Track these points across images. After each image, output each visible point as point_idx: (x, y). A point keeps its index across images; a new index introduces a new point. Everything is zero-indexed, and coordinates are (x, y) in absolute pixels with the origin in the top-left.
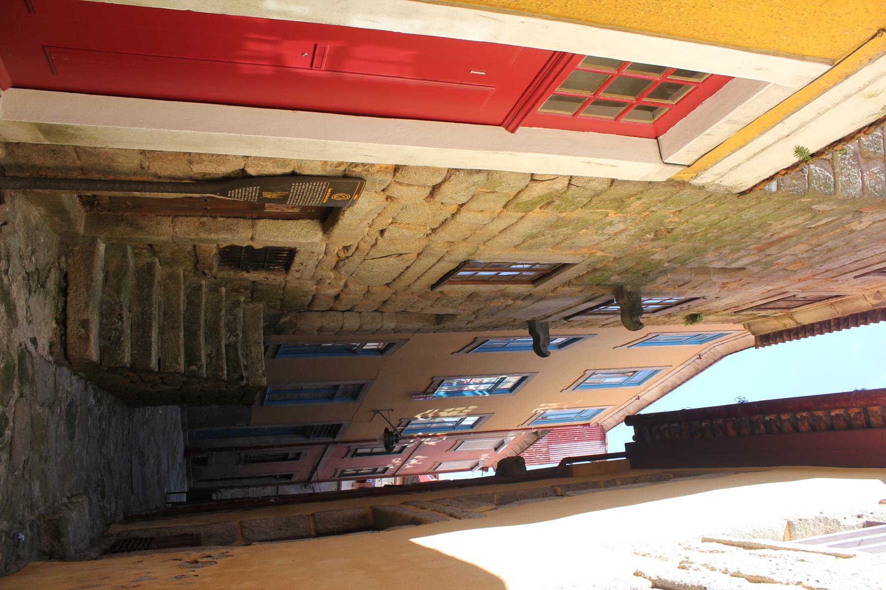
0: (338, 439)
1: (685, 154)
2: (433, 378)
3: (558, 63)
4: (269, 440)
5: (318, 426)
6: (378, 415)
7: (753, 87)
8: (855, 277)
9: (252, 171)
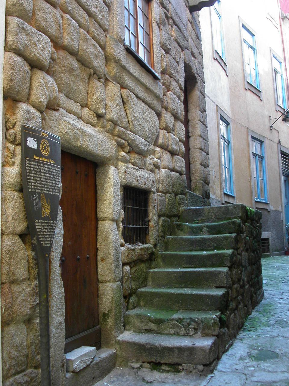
6: (274, 126)
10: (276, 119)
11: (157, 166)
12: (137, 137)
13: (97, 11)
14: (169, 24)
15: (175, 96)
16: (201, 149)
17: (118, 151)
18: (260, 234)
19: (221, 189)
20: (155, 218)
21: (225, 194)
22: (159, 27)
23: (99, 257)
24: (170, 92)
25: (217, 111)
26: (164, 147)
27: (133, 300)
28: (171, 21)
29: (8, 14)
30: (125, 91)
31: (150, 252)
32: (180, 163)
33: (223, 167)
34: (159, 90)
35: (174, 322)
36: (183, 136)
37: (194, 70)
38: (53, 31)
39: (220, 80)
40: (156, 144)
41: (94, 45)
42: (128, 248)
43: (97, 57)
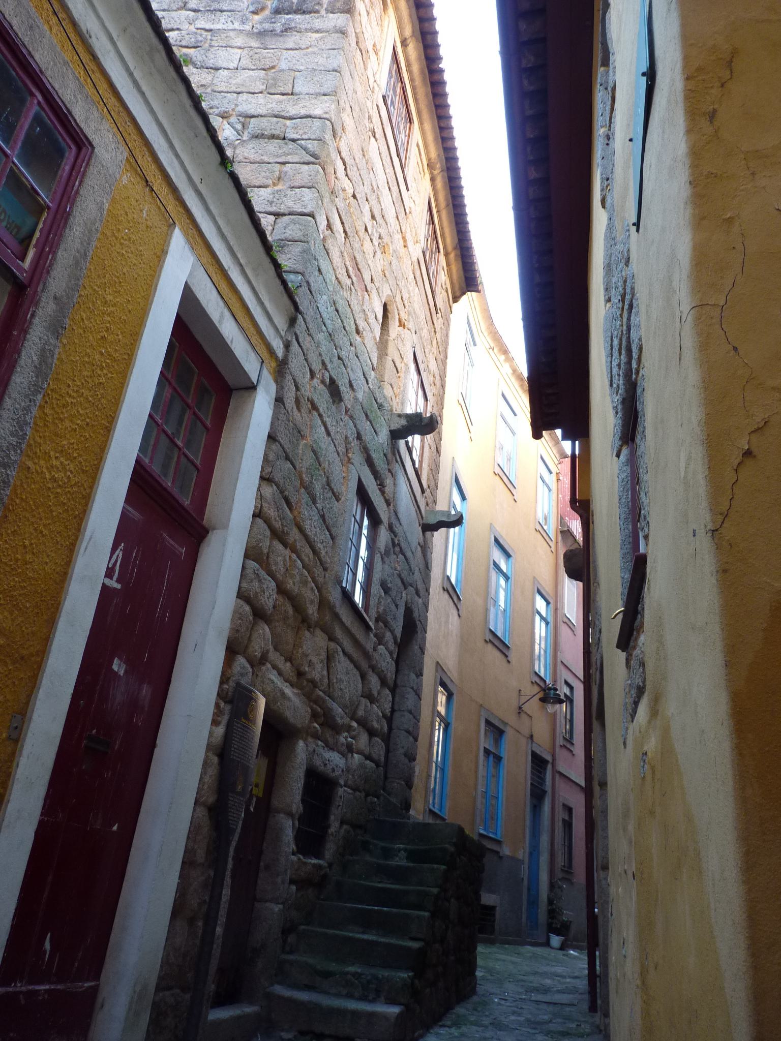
0: (548, 758)
1: (250, 363)
2: (486, 641)
3: (142, 482)
4: (545, 839)
5: (532, 779)
6: (525, 708)
7: (188, 297)
8: (408, 190)
9: (211, 799)
10: (528, 698)
11: (350, 749)
12: (335, 706)
13: (322, 547)
14: (394, 553)
15: (387, 653)
16: (408, 732)
17: (310, 722)
18: (478, 898)
19: (426, 801)
20: (337, 824)
21: (430, 811)
22: (382, 559)
23: (262, 864)
24: (382, 647)
25: (437, 671)
26: (363, 723)
27: (291, 939)
28: (397, 549)
29: (247, 556)
30: (332, 645)
31: (322, 873)
32: (379, 749)
33: (434, 764)
34: (369, 643)
35: (349, 977)
36: (387, 707)
37: (416, 615)
38: (280, 577)
39: (447, 622)
40: (353, 718)
41: (312, 589)
42: (299, 859)
43: (312, 602)
